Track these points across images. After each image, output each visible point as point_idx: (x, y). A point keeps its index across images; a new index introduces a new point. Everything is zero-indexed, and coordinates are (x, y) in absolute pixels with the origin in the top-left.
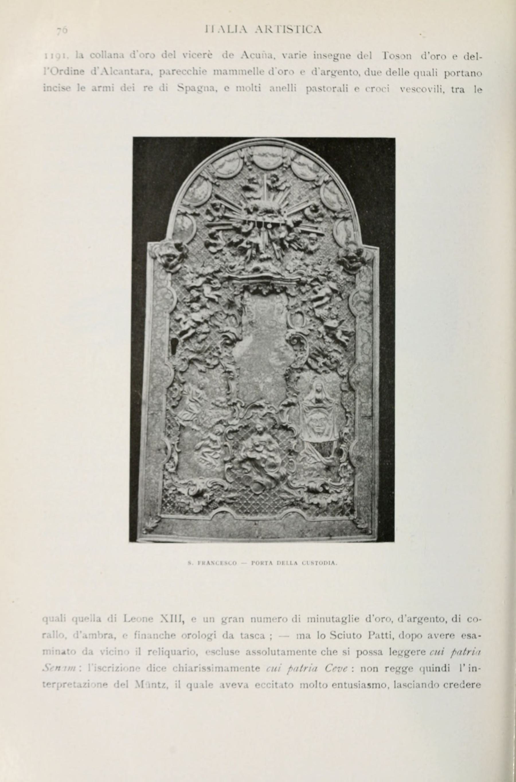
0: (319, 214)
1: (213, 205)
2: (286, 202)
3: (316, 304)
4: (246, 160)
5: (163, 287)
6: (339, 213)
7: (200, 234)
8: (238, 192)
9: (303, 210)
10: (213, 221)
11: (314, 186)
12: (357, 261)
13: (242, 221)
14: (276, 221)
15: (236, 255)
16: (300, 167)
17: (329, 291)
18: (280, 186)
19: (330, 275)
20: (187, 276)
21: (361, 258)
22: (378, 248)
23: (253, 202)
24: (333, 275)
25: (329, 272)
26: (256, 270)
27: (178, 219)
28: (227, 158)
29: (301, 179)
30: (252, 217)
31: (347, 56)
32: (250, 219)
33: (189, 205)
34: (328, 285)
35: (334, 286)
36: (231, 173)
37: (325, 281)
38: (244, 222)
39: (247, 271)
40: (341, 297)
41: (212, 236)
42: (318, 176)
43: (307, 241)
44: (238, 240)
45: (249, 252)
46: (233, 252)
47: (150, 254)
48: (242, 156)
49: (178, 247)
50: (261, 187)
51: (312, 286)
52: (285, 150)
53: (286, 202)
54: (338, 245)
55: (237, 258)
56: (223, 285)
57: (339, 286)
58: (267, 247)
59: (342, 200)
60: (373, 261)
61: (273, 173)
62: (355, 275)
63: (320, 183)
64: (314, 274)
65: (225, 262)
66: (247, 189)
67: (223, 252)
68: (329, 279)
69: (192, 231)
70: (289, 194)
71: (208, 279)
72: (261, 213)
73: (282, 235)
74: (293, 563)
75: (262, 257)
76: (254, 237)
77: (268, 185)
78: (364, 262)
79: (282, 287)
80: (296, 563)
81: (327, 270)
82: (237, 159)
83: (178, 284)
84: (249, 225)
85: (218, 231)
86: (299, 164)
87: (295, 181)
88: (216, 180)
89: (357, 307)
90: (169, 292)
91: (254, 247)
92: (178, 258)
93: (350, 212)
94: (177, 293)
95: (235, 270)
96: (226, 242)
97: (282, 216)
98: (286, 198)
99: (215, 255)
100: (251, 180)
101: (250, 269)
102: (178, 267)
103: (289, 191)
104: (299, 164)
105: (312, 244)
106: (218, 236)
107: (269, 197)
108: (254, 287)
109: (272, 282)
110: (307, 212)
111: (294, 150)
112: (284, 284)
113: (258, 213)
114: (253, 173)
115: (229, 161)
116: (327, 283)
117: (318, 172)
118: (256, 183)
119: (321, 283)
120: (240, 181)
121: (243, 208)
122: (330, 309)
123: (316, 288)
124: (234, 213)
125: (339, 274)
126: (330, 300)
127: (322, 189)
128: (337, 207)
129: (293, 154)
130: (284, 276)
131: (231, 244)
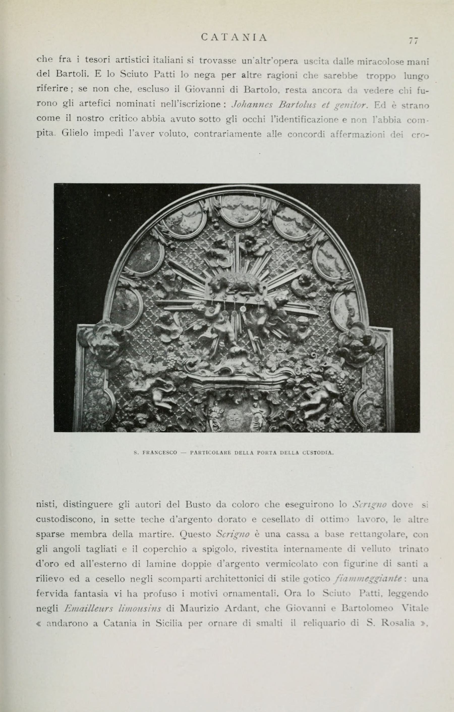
0: (311, 288)
1: (167, 278)
2: (267, 272)
3: (307, 414)
4: (211, 215)
5: (98, 388)
6: (339, 284)
7: (149, 316)
8: (200, 259)
9: (290, 283)
10: (165, 298)
11: (304, 249)
12: (364, 352)
13: (205, 303)
14: (252, 301)
15: (197, 347)
16: (286, 223)
17: (325, 395)
18: (257, 251)
19: (327, 372)
20: (130, 375)
21: (369, 347)
22: (391, 329)
23: (221, 274)
24: (331, 371)
25: (326, 368)
26: (225, 371)
27: (118, 294)
28: (185, 211)
29: (286, 240)
30: (219, 297)
31: (384, 609)
32: (216, 300)
33: (134, 275)
34: (325, 387)
35: (330, 387)
36: (191, 232)
37: (320, 380)
38: (209, 303)
39: (212, 371)
40: (343, 403)
41: (165, 320)
42: (309, 235)
43: (294, 327)
44: (200, 327)
45: (215, 343)
46: (193, 343)
47: (80, 343)
48: (206, 209)
49: (117, 335)
50: (231, 252)
51: (304, 389)
52: (264, 201)
53: (267, 272)
54: (337, 328)
55: (198, 351)
56: (180, 389)
57: (338, 387)
58: (240, 335)
59: (342, 266)
60: (384, 348)
61: (249, 233)
62: (361, 369)
63: (313, 244)
64: (305, 371)
65: (182, 357)
66: (211, 256)
67: (180, 343)
68: (326, 377)
69: (137, 311)
70: (271, 260)
71: (158, 381)
72: (231, 290)
73: (261, 321)
74: (295, 452)
75: (233, 350)
76: (222, 323)
77: (240, 249)
78: (373, 351)
79: (261, 392)
80: (297, 452)
81: (323, 365)
82: (199, 213)
83: (118, 385)
84: (215, 307)
85: (173, 312)
86: (284, 218)
87: (277, 243)
88: (171, 242)
89: (364, 413)
90: (105, 395)
91: (221, 339)
92: (118, 350)
93: (353, 283)
94: (116, 397)
95: (196, 367)
96: (184, 327)
97: (261, 294)
98: (265, 269)
99: (169, 347)
100: (218, 244)
101: (218, 368)
102: (120, 360)
103: (270, 256)
104: (284, 218)
105: (303, 331)
106: (173, 320)
107: (243, 265)
108: (222, 393)
109: (248, 387)
110: (295, 285)
111: (277, 201)
112: (264, 389)
113: (227, 290)
114: (221, 232)
115: (189, 216)
116: (324, 383)
117: (309, 229)
118: (223, 248)
119: (315, 384)
120: (203, 242)
121: (207, 281)
122: (327, 420)
123: (308, 392)
124: (194, 287)
125: (339, 369)
126: (328, 407)
127: (315, 251)
128: (335, 276)
129: (275, 206)
130: (263, 378)
131: (190, 332)
